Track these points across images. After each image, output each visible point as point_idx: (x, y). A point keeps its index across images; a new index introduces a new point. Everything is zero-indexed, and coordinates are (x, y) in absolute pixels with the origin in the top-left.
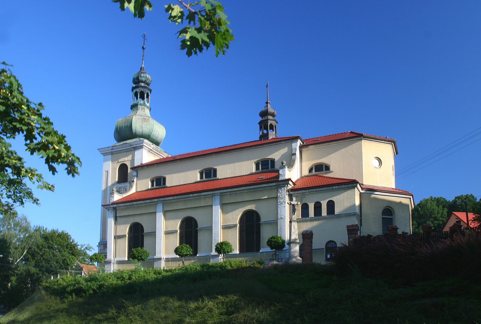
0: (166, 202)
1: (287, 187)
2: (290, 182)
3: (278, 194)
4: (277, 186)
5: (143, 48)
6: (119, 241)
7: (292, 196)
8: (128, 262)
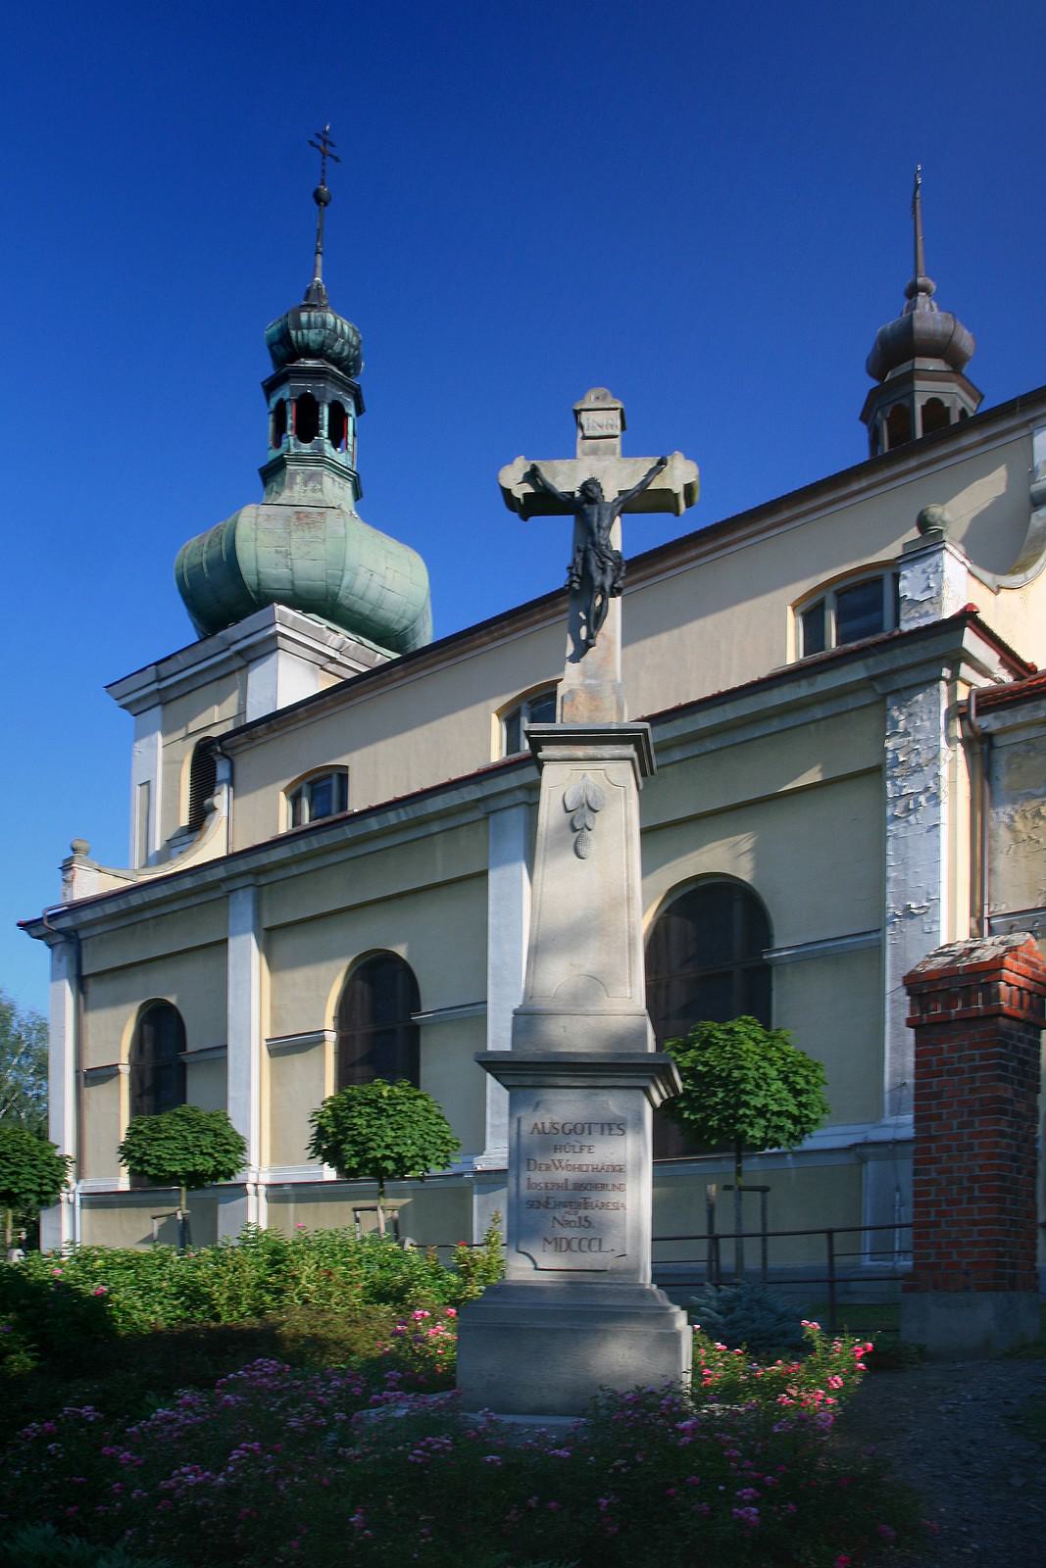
0: (272, 878)
1: (952, 682)
2: (971, 641)
3: (889, 744)
4: (879, 689)
5: (318, 198)
6: (95, 1094)
7: (992, 746)
8: (130, 1198)
